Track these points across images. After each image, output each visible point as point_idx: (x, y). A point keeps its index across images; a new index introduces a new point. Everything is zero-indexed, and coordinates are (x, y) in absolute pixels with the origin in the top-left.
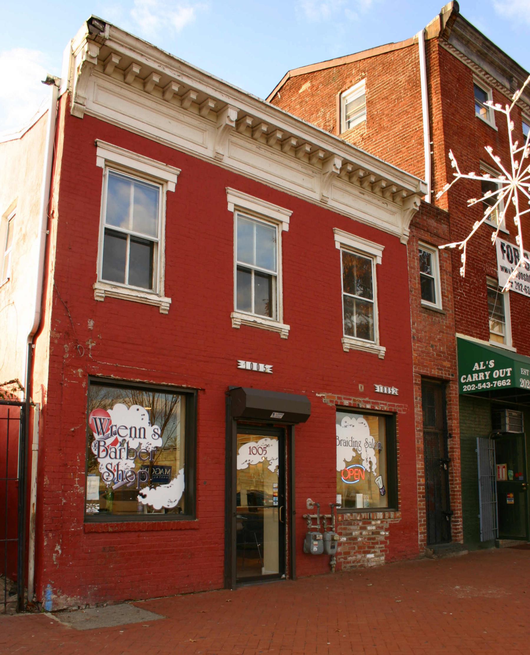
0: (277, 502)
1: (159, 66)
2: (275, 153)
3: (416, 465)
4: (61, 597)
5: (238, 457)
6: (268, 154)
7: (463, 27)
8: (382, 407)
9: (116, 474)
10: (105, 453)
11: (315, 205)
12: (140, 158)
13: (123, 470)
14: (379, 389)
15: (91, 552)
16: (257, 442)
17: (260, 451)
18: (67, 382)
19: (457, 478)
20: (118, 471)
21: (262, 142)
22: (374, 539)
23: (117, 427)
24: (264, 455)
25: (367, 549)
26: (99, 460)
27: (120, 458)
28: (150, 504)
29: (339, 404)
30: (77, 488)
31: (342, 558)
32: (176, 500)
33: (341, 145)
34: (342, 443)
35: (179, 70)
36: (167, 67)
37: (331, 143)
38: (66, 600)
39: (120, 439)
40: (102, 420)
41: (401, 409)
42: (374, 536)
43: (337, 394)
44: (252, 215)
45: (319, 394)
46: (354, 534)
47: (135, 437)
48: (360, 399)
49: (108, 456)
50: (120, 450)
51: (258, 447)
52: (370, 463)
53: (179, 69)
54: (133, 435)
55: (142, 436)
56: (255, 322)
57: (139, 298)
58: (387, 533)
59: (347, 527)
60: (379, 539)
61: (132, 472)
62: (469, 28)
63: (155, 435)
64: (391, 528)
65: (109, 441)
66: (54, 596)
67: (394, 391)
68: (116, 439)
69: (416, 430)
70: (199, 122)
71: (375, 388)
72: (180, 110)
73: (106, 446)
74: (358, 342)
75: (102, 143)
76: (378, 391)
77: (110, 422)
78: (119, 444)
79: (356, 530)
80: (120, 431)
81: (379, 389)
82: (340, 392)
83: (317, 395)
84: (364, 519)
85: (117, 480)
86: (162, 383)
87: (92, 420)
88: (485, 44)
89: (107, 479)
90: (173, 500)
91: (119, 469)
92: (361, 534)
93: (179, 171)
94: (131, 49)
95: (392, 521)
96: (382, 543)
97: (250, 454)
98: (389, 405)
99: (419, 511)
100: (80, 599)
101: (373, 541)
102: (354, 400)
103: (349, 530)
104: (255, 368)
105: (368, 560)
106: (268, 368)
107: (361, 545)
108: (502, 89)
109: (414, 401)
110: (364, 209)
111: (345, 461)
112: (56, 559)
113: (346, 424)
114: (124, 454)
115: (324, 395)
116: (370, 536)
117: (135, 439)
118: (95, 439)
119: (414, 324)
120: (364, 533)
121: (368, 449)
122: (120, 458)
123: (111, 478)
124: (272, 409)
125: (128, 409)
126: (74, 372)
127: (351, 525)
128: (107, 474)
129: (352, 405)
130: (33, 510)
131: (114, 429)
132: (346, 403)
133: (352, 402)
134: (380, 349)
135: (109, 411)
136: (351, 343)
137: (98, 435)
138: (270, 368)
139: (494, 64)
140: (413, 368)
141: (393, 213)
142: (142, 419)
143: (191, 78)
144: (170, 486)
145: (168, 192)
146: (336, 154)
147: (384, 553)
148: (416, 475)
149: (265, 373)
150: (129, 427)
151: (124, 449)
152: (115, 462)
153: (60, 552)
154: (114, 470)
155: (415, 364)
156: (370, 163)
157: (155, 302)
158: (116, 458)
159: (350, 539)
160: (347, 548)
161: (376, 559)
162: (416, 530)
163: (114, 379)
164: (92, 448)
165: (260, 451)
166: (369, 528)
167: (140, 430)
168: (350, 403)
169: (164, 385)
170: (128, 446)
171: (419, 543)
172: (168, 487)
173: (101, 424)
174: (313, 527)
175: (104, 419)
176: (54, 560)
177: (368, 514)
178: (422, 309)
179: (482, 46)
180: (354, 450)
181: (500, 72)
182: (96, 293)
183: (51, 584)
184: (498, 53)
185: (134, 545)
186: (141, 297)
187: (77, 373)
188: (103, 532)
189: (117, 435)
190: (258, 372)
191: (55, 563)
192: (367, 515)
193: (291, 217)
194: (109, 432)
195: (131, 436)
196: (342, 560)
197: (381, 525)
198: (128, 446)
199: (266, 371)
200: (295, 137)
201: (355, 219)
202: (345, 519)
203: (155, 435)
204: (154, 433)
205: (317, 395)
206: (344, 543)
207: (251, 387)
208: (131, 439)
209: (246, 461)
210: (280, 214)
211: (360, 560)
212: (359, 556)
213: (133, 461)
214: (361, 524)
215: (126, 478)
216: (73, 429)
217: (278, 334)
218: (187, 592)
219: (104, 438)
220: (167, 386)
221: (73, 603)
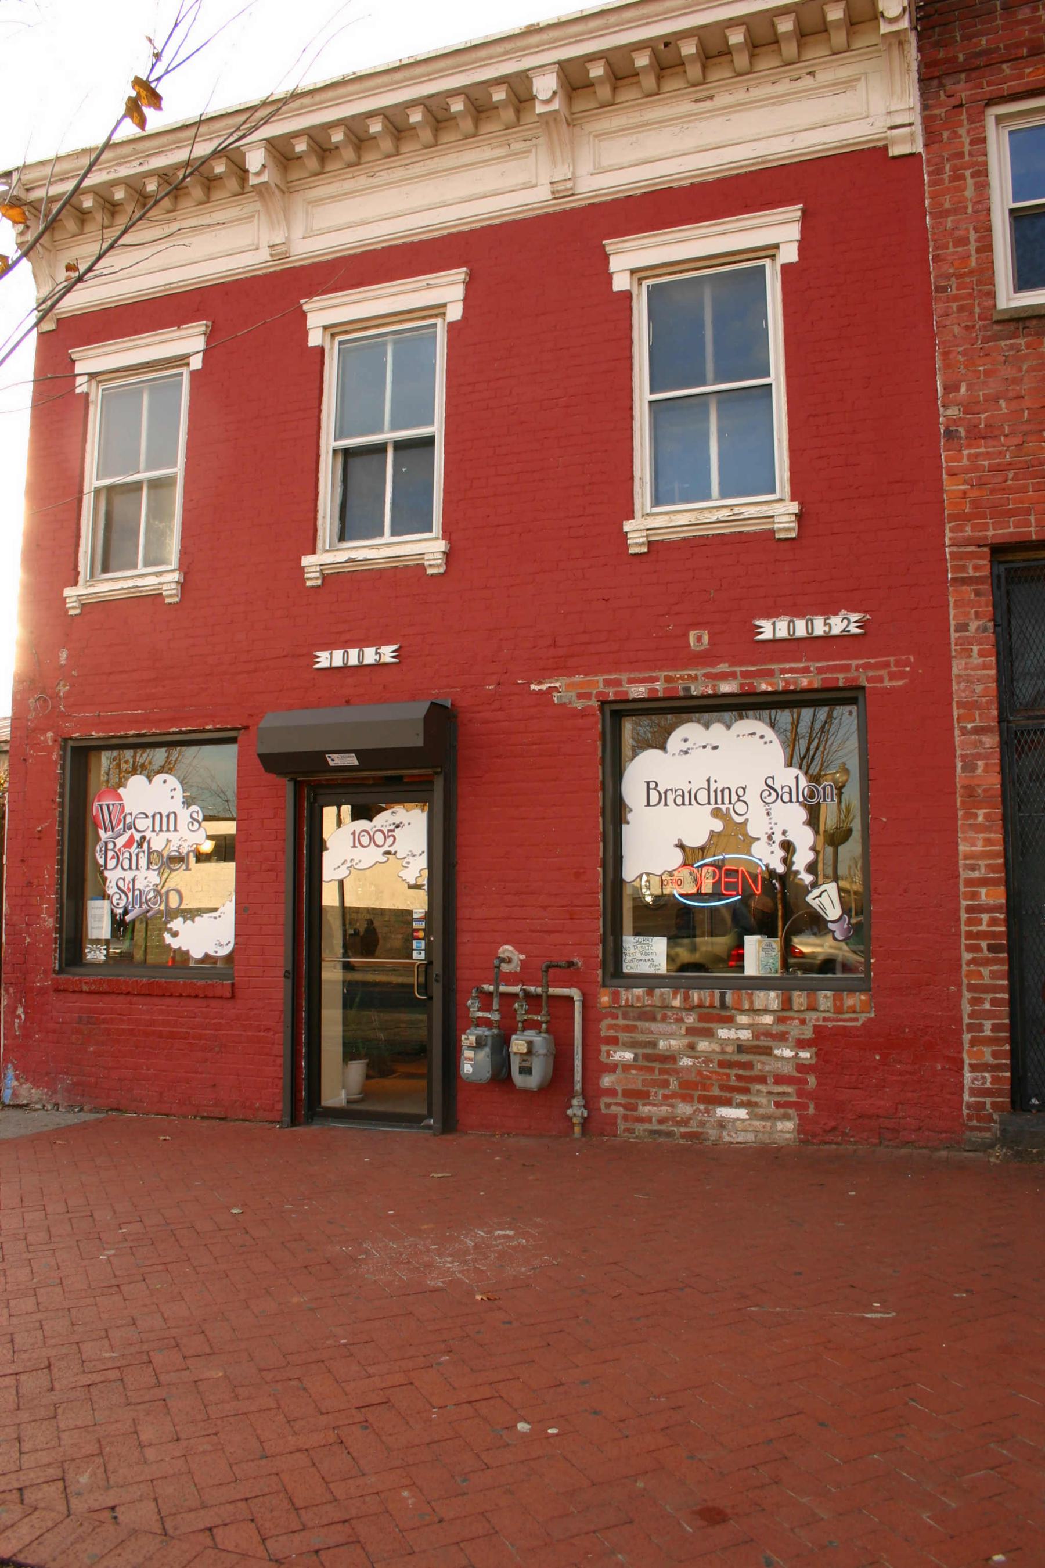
0: (423, 953)
1: (108, 173)
2: (414, 160)
3: (957, 844)
4: (24, 1086)
5: (325, 853)
6: (399, 174)
8: (787, 682)
9: (130, 895)
10: (115, 861)
11: (547, 215)
13: (142, 888)
15: (63, 1023)
17: (379, 838)
20: (134, 890)
21: (374, 158)
22: (749, 1065)
23: (134, 816)
24: (390, 846)
25: (716, 1092)
26: (107, 873)
27: (137, 868)
28: (184, 948)
30: (44, 920)
31: (618, 1104)
32: (229, 942)
33: (535, 39)
34: (670, 797)
35: (138, 154)
36: (120, 164)
38: (29, 1091)
40: (111, 807)
41: (884, 673)
42: (744, 1058)
43: (603, 673)
44: (377, 326)
45: (540, 683)
46: (662, 1044)
47: (161, 830)
50: (137, 855)
51: (374, 829)
52: (788, 846)
54: (157, 828)
55: (172, 828)
56: (351, 560)
57: (126, 591)
58: (805, 1055)
59: (638, 1023)
60: (767, 1068)
61: (155, 890)
63: (193, 824)
65: (121, 841)
66: (16, 1083)
68: (132, 836)
69: (957, 732)
71: (755, 630)
72: (200, 210)
73: (116, 850)
74: (679, 516)
75: (192, 327)
77: (123, 808)
78: (135, 845)
79: (671, 1034)
80: (137, 821)
82: (617, 666)
83: (533, 687)
84: (700, 1006)
85: (133, 906)
87: (97, 808)
89: (118, 904)
90: (224, 942)
91: (136, 887)
92: (692, 1047)
93: (203, 325)
94: (62, 180)
95: (825, 1019)
96: (780, 1080)
97: (354, 846)
98: (820, 671)
99: (967, 995)
100: (47, 1094)
101: (741, 1072)
104: (353, 661)
105: (722, 1124)
106: (387, 653)
109: (949, 635)
110: (642, 155)
111: (681, 846)
112: (19, 1027)
113: (685, 746)
114: (143, 862)
115: (557, 685)
116: (728, 1057)
117: (161, 834)
118: (100, 839)
120: (703, 1045)
122: (137, 868)
123: (123, 903)
124: (323, 749)
125: (150, 781)
126: (42, 738)
127: (654, 1019)
128: (117, 896)
129: (660, 694)
131: (129, 820)
132: (638, 691)
133: (659, 686)
134: (771, 513)
136: (648, 527)
137: (106, 831)
140: (947, 531)
141: (847, 84)
142: (172, 797)
143: (159, 152)
146: (529, 70)
147: (791, 1112)
148: (958, 876)
149: (379, 666)
150: (150, 815)
151: (144, 852)
153: (23, 1017)
154: (129, 888)
155: (953, 517)
156: (649, 17)
157: (152, 588)
158: (130, 868)
159: (647, 1057)
160: (636, 1080)
161: (758, 1124)
162: (951, 1053)
164: (97, 854)
165: (379, 838)
166: (723, 1033)
167: (168, 816)
169: (174, 733)
170: (149, 848)
171: (966, 1097)
172: (215, 918)
173: (110, 814)
174: (480, 1014)
175: (113, 805)
176: (17, 1029)
177: (717, 992)
178: (996, 327)
180: (716, 813)
183: (12, 1063)
185: (125, 1018)
187: (46, 739)
188: (74, 992)
189: (133, 830)
190: (361, 667)
191: (17, 1033)
192: (712, 996)
194: (121, 825)
195: (153, 830)
196: (619, 1111)
197: (775, 1029)
198: (149, 848)
199: (382, 661)
200: (297, 136)
201: (687, 183)
202: (623, 1003)
203: (193, 824)
204: (190, 820)
206: (627, 1067)
207: (348, 702)
209: (345, 862)
210: (433, 290)
211: (689, 1119)
212: (684, 1109)
213: (157, 872)
214: (691, 1019)
215: (147, 901)
216: (39, 829)
217: (156, 597)
218: (212, 1115)
219: (114, 836)
220: (181, 732)
221: (35, 1098)
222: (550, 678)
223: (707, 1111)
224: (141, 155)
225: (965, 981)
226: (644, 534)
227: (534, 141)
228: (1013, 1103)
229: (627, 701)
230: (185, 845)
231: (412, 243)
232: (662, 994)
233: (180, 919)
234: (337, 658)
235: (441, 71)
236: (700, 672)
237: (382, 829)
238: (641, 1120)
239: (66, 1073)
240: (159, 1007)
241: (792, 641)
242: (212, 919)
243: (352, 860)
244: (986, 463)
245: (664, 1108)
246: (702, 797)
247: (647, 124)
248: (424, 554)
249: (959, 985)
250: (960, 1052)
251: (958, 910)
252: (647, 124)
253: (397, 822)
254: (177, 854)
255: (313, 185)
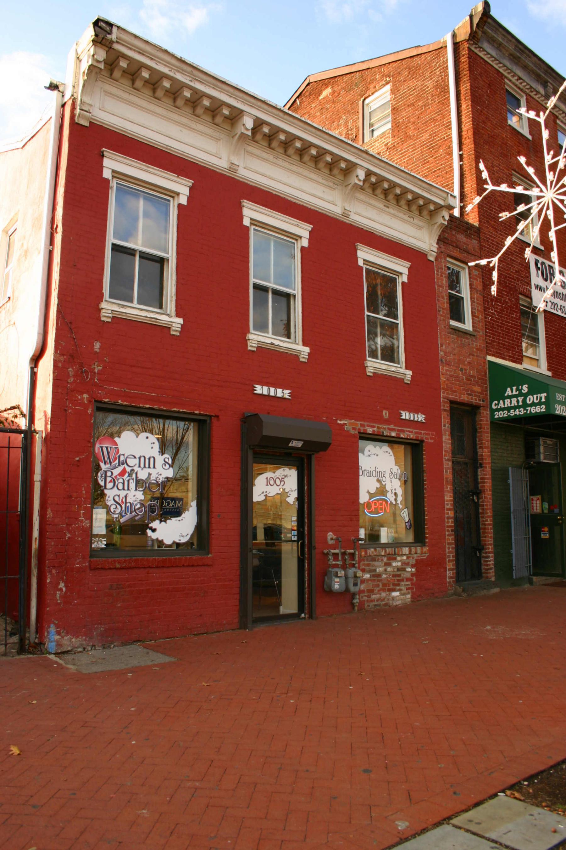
0: (296, 537)
1: (170, 71)
2: (294, 163)
4: (66, 638)
5: (254, 488)
6: (287, 165)
7: (494, 29)
9: (123, 506)
10: (112, 484)
11: (337, 220)
12: (149, 169)
13: (132, 502)
14: (405, 415)
16: (274, 472)
17: (278, 482)
18: (71, 408)
19: (488, 511)
20: (126, 503)
21: (280, 152)
22: (399, 576)
24: (282, 486)
25: (391, 587)
26: (106, 491)
27: (128, 489)
28: (160, 539)
29: (362, 431)
30: (82, 521)
31: (365, 596)
32: (188, 534)
35: (191, 74)
36: (178, 71)
37: (354, 153)
38: (70, 641)
39: (128, 469)
40: (109, 449)
41: (429, 437)
44: (269, 230)
45: (340, 420)
46: (378, 570)
47: (145, 467)
48: (385, 427)
49: (116, 487)
50: (128, 481)
51: (276, 477)
53: (191, 73)
54: (142, 465)
55: (152, 466)
56: (272, 344)
57: (148, 319)
58: (414, 570)
59: (371, 563)
60: (404, 576)
61: (141, 504)
62: (501, 30)
63: (165, 465)
64: (418, 564)
65: (116, 472)
66: (58, 637)
67: (420, 418)
68: (124, 469)
69: (444, 460)
70: (213, 131)
71: (400, 415)
73: (113, 476)
75: (109, 152)
76: (403, 417)
77: (118, 451)
78: (127, 475)
79: (380, 566)
81: (405, 415)
82: (363, 419)
83: (339, 422)
84: (389, 554)
85: (125, 513)
86: (173, 409)
87: (99, 448)
88: (518, 47)
89: (115, 511)
90: (185, 535)
91: (128, 501)
92: (386, 570)
93: (191, 182)
94: (140, 53)
96: (408, 580)
97: (267, 485)
98: (416, 433)
99: (447, 546)
100: (85, 640)
101: (398, 578)
102: (378, 428)
103: (372, 566)
104: (272, 394)
105: (393, 598)
106: (286, 394)
107: (385, 582)
108: (536, 95)
109: (442, 428)
111: (368, 492)
112: (60, 597)
113: (369, 453)
114: (133, 485)
115: (346, 422)
117: (144, 469)
118: (101, 469)
119: (442, 346)
120: (389, 569)
121: (393, 480)
122: (128, 489)
123: (118, 511)
124: (291, 437)
125: (137, 437)
126: (79, 397)
128: (114, 507)
129: (376, 433)
130: (35, 545)
131: (122, 458)
132: (370, 430)
133: (375, 429)
134: (405, 373)
135: (116, 439)
137: (105, 464)
138: (289, 393)
139: (527, 68)
140: (441, 393)
141: (420, 228)
142: (152, 448)
143: (204, 83)
144: (182, 520)
145: (180, 206)
147: (410, 591)
148: (444, 507)
149: (283, 398)
150: (137, 456)
151: (133, 479)
152: (122, 494)
153: (64, 589)
154: (122, 502)
156: (396, 174)
157: (166, 322)
158: (124, 489)
159: (374, 576)
160: (370, 585)
161: (402, 597)
163: (122, 405)
164: (99, 479)
165: (278, 482)
166: (394, 564)
167: (149, 459)
168: (374, 431)
169: (175, 412)
170: (137, 477)
171: (448, 580)
172: (179, 521)
173: (108, 453)
174: (334, 563)
175: (111, 448)
176: (58, 598)
177: (393, 549)
179: (515, 49)
180: (378, 481)
181: (534, 77)
182: (103, 313)
183: (54, 624)
184: (532, 56)
185: (143, 582)
186: (151, 318)
187: (83, 398)
188: (110, 569)
189: (125, 465)
190: (275, 397)
191: (59, 601)
192: (392, 550)
193: (310, 232)
194: (117, 461)
195: (140, 466)
197: (407, 561)
198: (137, 477)
199: (284, 397)
201: (379, 234)
202: (368, 554)
203: (165, 465)
204: (164, 463)
205: (339, 422)
206: (368, 580)
207: (269, 413)
208: (140, 469)
209: (263, 493)
212: (383, 594)
215: (135, 510)
216: (78, 459)
217: (297, 357)
218: (200, 632)
220: (178, 412)
221: (78, 644)
222: (344, 419)
223: (389, 594)
224: (192, 76)
225: (447, 542)
226: (257, 343)
227: (336, 186)
228: (456, 581)
229: (366, 434)
230: (160, 477)
231: (287, 200)
232: (379, 550)
233: (157, 522)
234: (280, 392)
235: (391, 171)
236: (386, 427)
237: (279, 477)
238: (372, 601)
239: (101, 624)
240: (166, 574)
241: (409, 421)
242: (178, 521)
243: (266, 492)
244: (449, 373)
245: (378, 595)
246: (374, 474)
247: (371, 204)
248: (174, 322)
249: (445, 543)
250: (446, 565)
251: (445, 518)
252: (371, 204)
253: (286, 475)
254: (155, 482)
255: (250, 144)
